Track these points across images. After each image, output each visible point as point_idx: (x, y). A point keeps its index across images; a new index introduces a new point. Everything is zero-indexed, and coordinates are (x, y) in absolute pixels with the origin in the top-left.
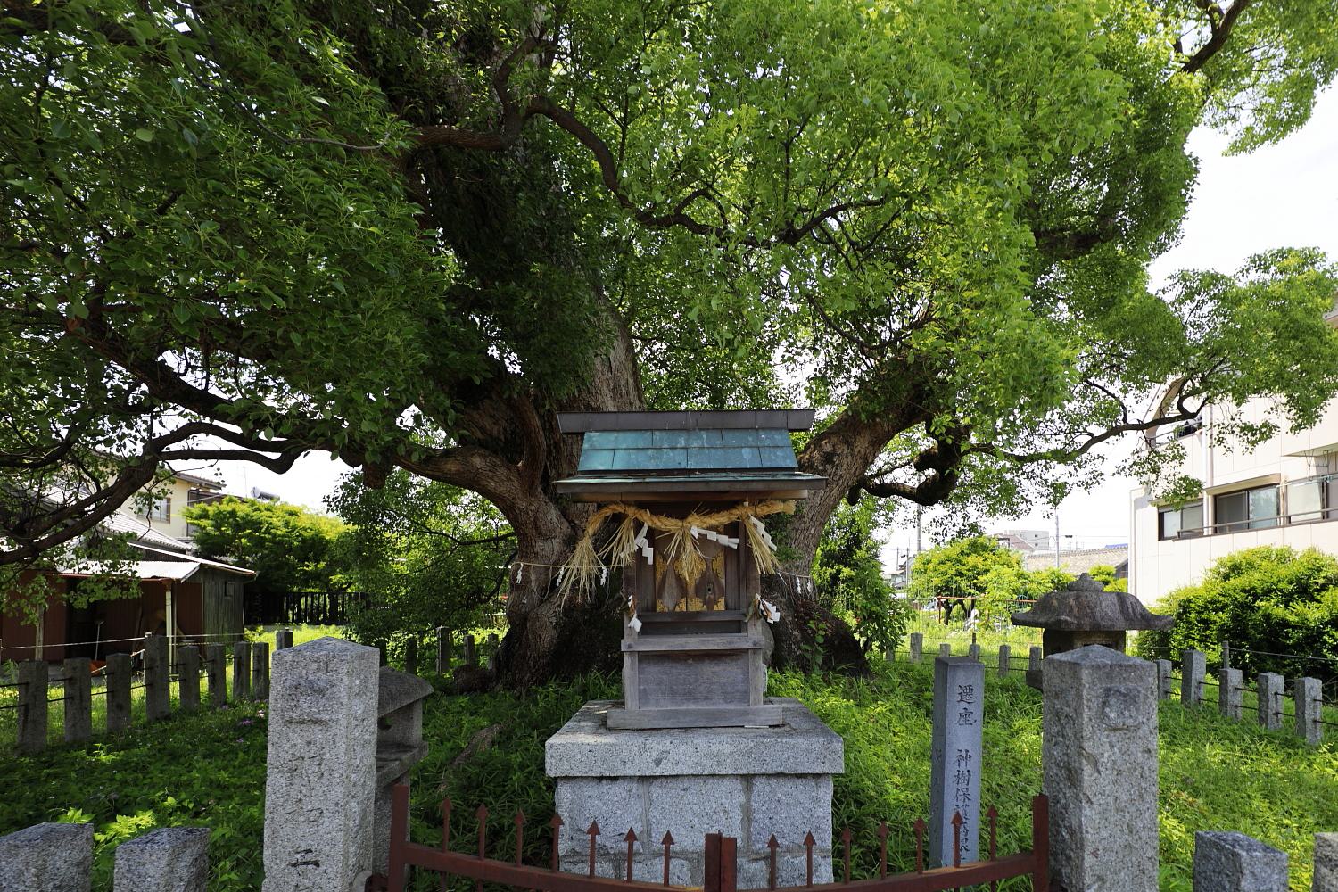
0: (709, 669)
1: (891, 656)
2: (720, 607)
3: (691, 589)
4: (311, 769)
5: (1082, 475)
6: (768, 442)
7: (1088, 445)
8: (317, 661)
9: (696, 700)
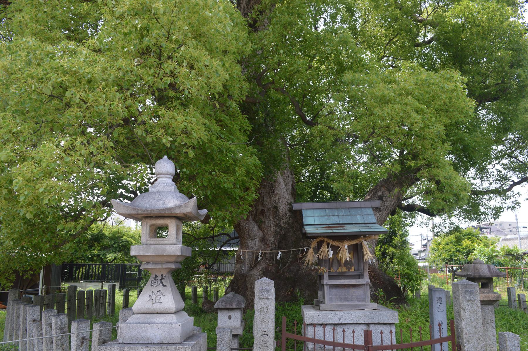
0: (352, 290)
1: (418, 295)
2: (352, 270)
3: (342, 264)
4: (265, 310)
5: (509, 203)
6: (365, 213)
7: (511, 187)
8: (266, 283)
9: (348, 301)
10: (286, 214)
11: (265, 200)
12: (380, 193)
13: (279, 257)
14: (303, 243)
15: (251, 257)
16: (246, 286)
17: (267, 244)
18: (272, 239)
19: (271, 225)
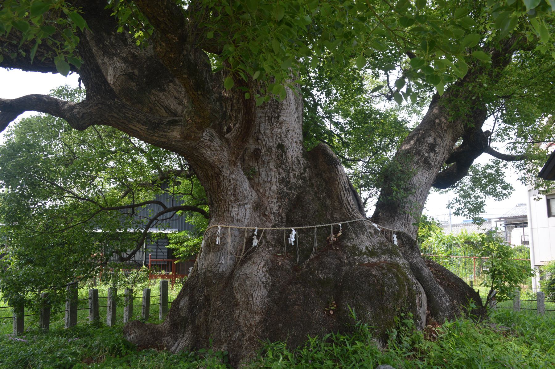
10: (299, 161)
11: (262, 131)
12: (430, 140)
13: (292, 238)
14: (331, 215)
15: (238, 239)
16: (234, 298)
17: (265, 215)
18: (275, 207)
19: (271, 178)
